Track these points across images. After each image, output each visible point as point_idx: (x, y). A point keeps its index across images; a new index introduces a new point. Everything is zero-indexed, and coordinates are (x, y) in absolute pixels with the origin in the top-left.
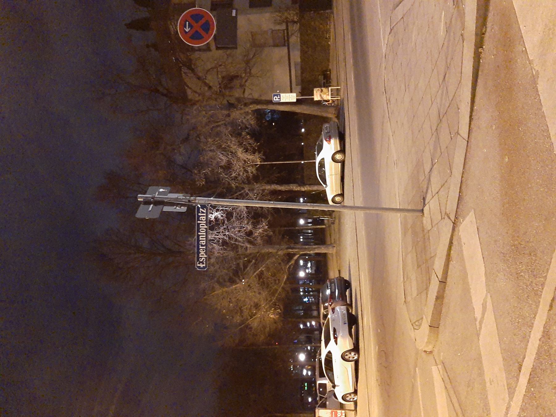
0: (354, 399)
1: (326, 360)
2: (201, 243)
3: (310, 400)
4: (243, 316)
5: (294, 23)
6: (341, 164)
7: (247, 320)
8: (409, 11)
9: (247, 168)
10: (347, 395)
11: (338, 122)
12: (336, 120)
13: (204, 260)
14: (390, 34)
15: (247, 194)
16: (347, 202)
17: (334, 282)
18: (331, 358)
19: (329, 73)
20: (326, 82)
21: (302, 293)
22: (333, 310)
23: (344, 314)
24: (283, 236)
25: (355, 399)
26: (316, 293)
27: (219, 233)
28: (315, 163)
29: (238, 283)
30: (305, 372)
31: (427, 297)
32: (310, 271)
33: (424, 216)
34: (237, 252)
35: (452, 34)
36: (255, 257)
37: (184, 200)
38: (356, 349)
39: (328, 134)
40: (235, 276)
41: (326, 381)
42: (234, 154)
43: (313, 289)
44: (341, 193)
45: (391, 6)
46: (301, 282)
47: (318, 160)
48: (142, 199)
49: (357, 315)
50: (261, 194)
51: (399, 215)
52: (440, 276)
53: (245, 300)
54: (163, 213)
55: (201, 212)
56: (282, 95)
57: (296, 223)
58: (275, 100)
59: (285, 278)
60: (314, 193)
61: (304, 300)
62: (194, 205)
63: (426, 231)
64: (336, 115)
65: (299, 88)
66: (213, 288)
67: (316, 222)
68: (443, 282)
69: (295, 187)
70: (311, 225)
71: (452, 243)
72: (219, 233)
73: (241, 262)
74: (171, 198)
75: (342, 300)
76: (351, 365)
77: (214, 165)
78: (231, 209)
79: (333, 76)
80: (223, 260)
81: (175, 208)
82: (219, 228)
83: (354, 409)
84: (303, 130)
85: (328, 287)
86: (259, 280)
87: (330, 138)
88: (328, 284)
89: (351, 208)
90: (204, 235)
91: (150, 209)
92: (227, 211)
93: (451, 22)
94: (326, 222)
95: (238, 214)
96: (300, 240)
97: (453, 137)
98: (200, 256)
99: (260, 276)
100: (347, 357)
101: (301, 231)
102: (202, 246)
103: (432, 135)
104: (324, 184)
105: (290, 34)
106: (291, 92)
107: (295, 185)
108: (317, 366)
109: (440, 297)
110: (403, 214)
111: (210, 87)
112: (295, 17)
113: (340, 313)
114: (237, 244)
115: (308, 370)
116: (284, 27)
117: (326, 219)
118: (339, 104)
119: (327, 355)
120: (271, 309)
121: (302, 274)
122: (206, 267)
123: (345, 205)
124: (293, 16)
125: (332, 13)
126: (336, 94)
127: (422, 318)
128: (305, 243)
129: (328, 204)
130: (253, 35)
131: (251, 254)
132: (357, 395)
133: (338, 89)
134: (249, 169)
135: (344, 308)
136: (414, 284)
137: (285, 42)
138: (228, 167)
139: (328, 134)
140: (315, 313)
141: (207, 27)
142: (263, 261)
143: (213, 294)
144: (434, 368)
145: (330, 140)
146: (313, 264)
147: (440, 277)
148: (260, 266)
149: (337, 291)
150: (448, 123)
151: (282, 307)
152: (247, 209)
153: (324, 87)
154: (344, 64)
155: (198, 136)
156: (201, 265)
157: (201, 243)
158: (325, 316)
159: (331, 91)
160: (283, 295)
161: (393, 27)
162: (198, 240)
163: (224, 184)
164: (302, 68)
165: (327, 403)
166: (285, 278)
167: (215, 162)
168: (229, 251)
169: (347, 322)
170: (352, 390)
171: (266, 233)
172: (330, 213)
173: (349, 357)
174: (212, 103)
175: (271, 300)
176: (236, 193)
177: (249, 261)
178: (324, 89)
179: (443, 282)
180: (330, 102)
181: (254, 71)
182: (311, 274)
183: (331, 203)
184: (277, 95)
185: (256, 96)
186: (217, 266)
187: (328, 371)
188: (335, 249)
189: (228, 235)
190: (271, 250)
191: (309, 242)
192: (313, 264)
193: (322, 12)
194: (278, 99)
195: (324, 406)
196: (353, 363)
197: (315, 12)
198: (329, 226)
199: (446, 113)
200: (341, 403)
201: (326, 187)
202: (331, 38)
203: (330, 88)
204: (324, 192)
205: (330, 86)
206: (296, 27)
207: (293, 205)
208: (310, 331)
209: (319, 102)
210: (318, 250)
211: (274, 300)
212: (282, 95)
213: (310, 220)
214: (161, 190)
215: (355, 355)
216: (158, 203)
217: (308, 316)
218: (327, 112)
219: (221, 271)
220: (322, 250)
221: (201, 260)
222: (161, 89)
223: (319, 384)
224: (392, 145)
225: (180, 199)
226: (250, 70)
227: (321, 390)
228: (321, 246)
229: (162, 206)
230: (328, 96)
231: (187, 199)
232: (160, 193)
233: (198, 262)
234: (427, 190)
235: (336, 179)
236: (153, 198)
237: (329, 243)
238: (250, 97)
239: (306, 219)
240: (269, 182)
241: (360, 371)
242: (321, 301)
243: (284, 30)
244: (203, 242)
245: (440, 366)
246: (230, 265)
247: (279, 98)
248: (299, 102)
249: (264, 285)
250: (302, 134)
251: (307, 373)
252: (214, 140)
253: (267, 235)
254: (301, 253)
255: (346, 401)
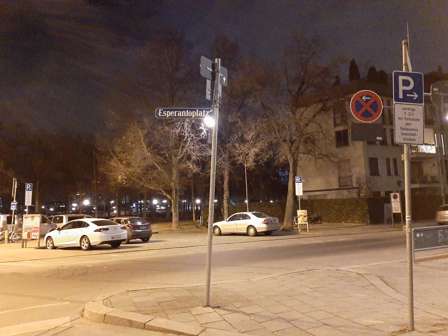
0: (49, 246)
1: (82, 222)
2: (179, 112)
3: (52, 209)
4: (120, 153)
5: (358, 193)
6: (245, 233)
7: (117, 157)
8: (378, 290)
9: (241, 156)
10: (51, 241)
11: (280, 230)
12: (281, 228)
13: (165, 115)
14: (357, 273)
15: (220, 156)
16: (214, 238)
17: (147, 228)
18: (83, 227)
19: (319, 222)
20: (312, 220)
21: (139, 202)
22: (124, 228)
23: (120, 237)
24: (187, 186)
25: (48, 248)
26: (139, 213)
27: (189, 133)
28: (246, 211)
29: (147, 149)
30: (74, 205)
31: (132, 312)
32: (158, 209)
33: (204, 307)
34: (173, 148)
35: (365, 331)
36: (169, 163)
37: (216, 97)
38: (91, 248)
39: (269, 222)
40: (153, 147)
41: (65, 221)
42: (254, 145)
43: (142, 212)
44: (221, 233)
45: (380, 274)
46: (148, 201)
47: (249, 214)
48: (217, 62)
49: (120, 249)
50: (220, 167)
51: (205, 284)
52: (151, 324)
53: (133, 155)
54: (205, 80)
55: (206, 112)
56: (301, 184)
57: (196, 196)
58: (297, 178)
59: (152, 188)
60: (222, 210)
61: (134, 204)
62: (212, 106)
63: (190, 309)
64: (285, 228)
65: (306, 198)
66: (144, 129)
67: (198, 213)
68: (144, 327)
69: (226, 195)
70: (196, 209)
71: (180, 334)
72: (189, 133)
73: (165, 152)
74: (218, 87)
75: (133, 236)
76: (78, 244)
77: (244, 129)
78: (209, 142)
79: (317, 226)
80: (166, 137)
81: (209, 90)
82: (193, 133)
83: (40, 246)
84: (272, 202)
85: (143, 223)
86: (150, 167)
87: (267, 223)
88: (146, 223)
89: (211, 243)
90: (186, 115)
91: (208, 68)
92: (207, 140)
93: (376, 330)
94: (198, 221)
95: (204, 149)
96: (183, 200)
97: (274, 334)
98: (168, 112)
99: (153, 168)
100: (84, 240)
101: (190, 200)
102: (177, 113)
103: (275, 314)
104: (229, 219)
105: (349, 190)
106: (304, 192)
107: (228, 196)
108: (78, 215)
109: (131, 324)
110: (205, 287)
111: (307, 125)
112: (363, 195)
113: (122, 233)
114: (179, 148)
115: (76, 207)
116: (355, 185)
117: (201, 221)
118: (294, 231)
119: (85, 223)
120: (126, 176)
121: (155, 202)
122: (158, 116)
123: (213, 237)
124: (364, 192)
125: (367, 225)
126: (302, 228)
127: (113, 307)
128: (180, 203)
129: (214, 223)
130: (348, 161)
131: (171, 159)
132: (51, 249)
133: (307, 230)
134: (241, 158)
135: (126, 237)
136: (144, 299)
137: (342, 187)
138: (243, 141)
139: (269, 222)
140: (123, 213)
141: (367, 115)
142: (166, 169)
143: (138, 129)
144: (68, 319)
145: (265, 224)
146: (164, 211)
147: (149, 323)
148: (162, 167)
149: (141, 231)
150: (287, 329)
151: (127, 185)
152: (209, 156)
153: (308, 218)
154: (328, 234)
155: (267, 116)
156: (160, 112)
157: (179, 112)
158: (119, 222)
159: (305, 224)
160: (137, 187)
161: (363, 276)
162: (181, 110)
163: (229, 137)
164: (323, 200)
165: (46, 224)
166: (152, 188)
167: (247, 130)
168: (175, 141)
169: (113, 240)
170: (56, 245)
171: (189, 171)
172: (205, 224)
173: (49, 243)
174: (294, 129)
175: (133, 176)
176: (221, 147)
177: (165, 158)
178: (306, 218)
179: (144, 327)
180: (296, 223)
181: (320, 161)
182: (155, 209)
183: (214, 224)
184: (300, 180)
185: (299, 163)
186: (162, 132)
187: (72, 224)
188: (176, 229)
189: (188, 140)
190: (174, 176)
191: (181, 208)
192: (164, 211)
193: (368, 216)
194: (298, 181)
195: (43, 221)
196: (79, 245)
197: (367, 210)
198: (194, 224)
199: (295, 326)
200: (45, 235)
201: (227, 221)
202: (348, 224)
203: (307, 223)
204: (222, 219)
205: (309, 223)
206: (355, 195)
207: (213, 191)
208: (108, 209)
209: (295, 214)
210: (174, 215)
211: (133, 178)
212: (301, 184)
213: (199, 208)
214: (224, 79)
215: (86, 247)
216: (214, 76)
217: (121, 207)
218: (288, 221)
219: (158, 135)
220: (175, 218)
221: (165, 112)
222: (304, 86)
223: (63, 217)
224: (263, 277)
225: (217, 95)
226: (321, 158)
227: (58, 218)
228: (178, 217)
229: (211, 79)
230: (301, 221)
231: (217, 100)
232: (222, 77)
233: (162, 110)
234: (226, 310)
235: (233, 229)
236: (218, 71)
237: (180, 224)
238: (299, 158)
239: (201, 205)
240: (230, 174)
241: (72, 251)
242: (132, 217)
243: (352, 185)
244: (180, 114)
245: (69, 324)
246: (163, 142)
247: (299, 181)
248: (295, 197)
249: (146, 171)
250: (268, 200)
251: (73, 207)
252: (264, 129)
253: (188, 173)
254: (172, 201)
255: (47, 239)
